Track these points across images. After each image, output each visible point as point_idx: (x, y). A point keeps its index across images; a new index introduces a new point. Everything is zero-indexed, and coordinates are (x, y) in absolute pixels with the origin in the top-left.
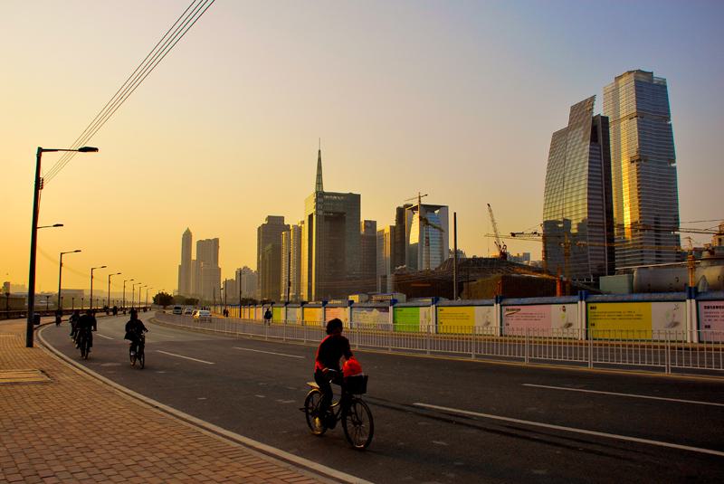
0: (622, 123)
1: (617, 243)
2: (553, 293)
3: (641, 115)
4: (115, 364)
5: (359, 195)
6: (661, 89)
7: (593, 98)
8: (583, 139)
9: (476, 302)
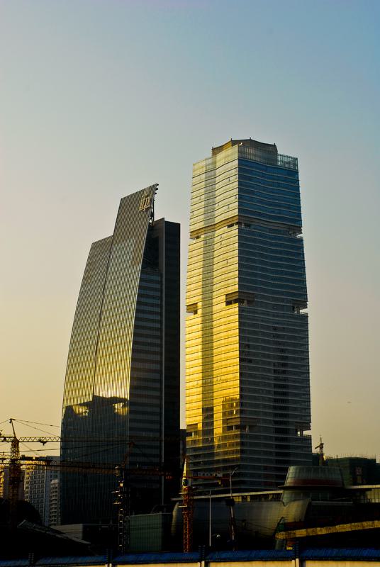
0: (217, 233)
1: (218, 454)
2: (180, 550)
3: (246, 221)
4: (196, 498)
5: (179, 224)
6: (289, 174)
7: (153, 189)
8: (134, 258)
9: (80, 560)
